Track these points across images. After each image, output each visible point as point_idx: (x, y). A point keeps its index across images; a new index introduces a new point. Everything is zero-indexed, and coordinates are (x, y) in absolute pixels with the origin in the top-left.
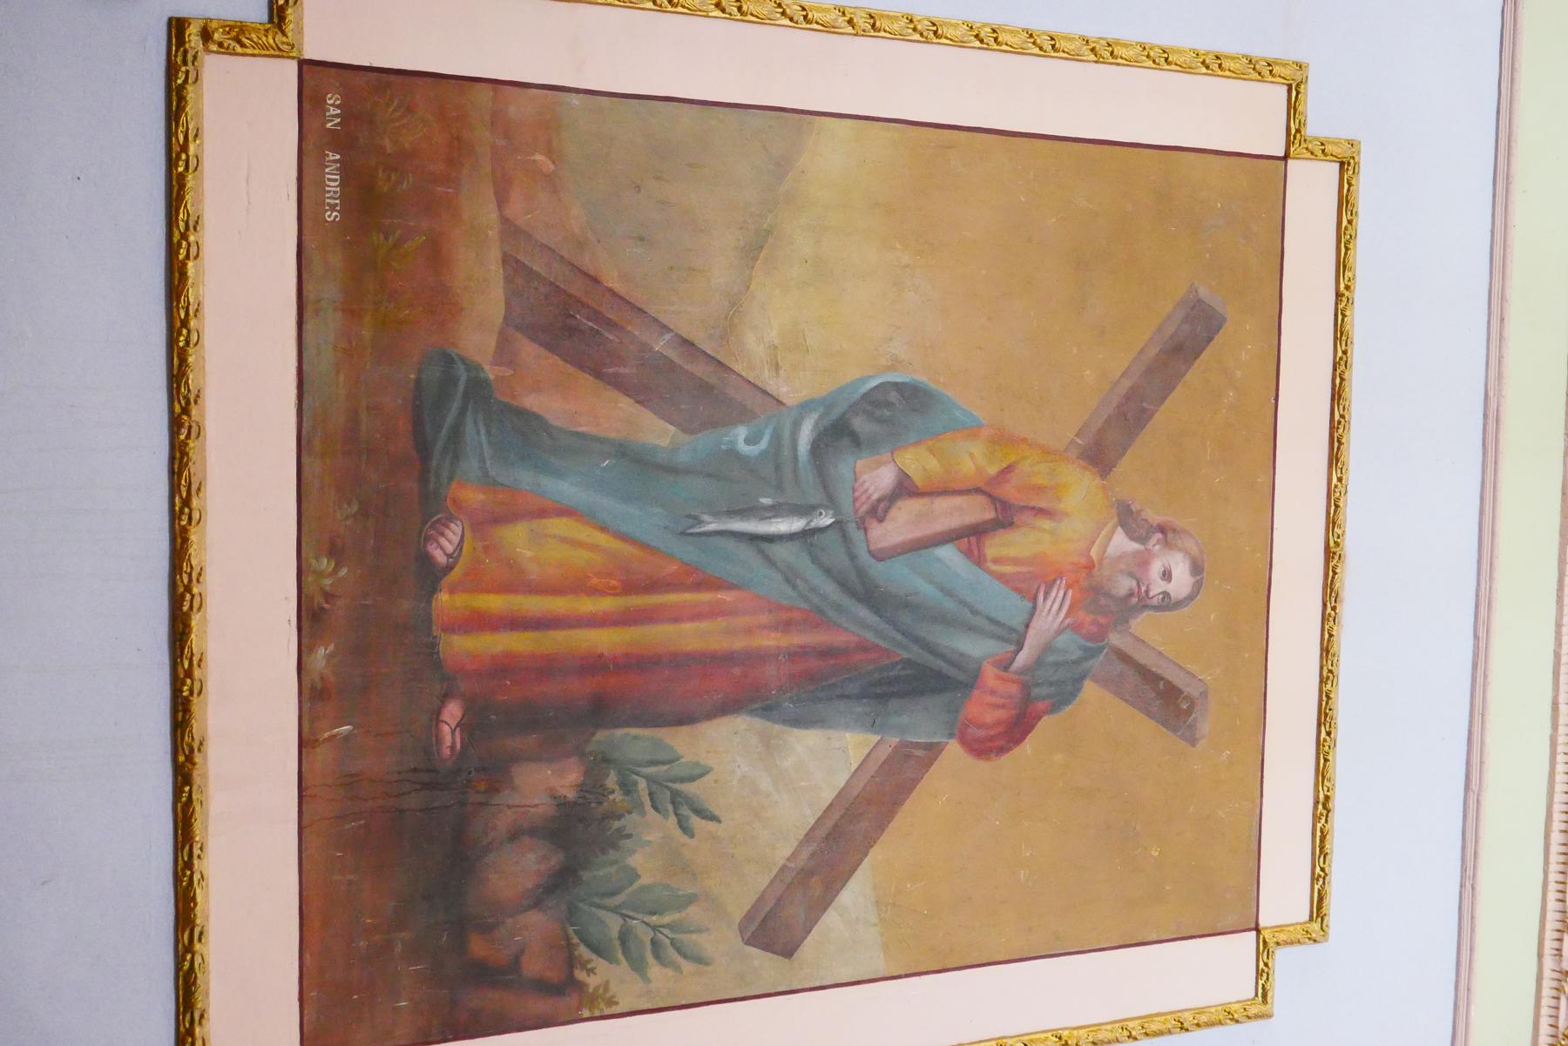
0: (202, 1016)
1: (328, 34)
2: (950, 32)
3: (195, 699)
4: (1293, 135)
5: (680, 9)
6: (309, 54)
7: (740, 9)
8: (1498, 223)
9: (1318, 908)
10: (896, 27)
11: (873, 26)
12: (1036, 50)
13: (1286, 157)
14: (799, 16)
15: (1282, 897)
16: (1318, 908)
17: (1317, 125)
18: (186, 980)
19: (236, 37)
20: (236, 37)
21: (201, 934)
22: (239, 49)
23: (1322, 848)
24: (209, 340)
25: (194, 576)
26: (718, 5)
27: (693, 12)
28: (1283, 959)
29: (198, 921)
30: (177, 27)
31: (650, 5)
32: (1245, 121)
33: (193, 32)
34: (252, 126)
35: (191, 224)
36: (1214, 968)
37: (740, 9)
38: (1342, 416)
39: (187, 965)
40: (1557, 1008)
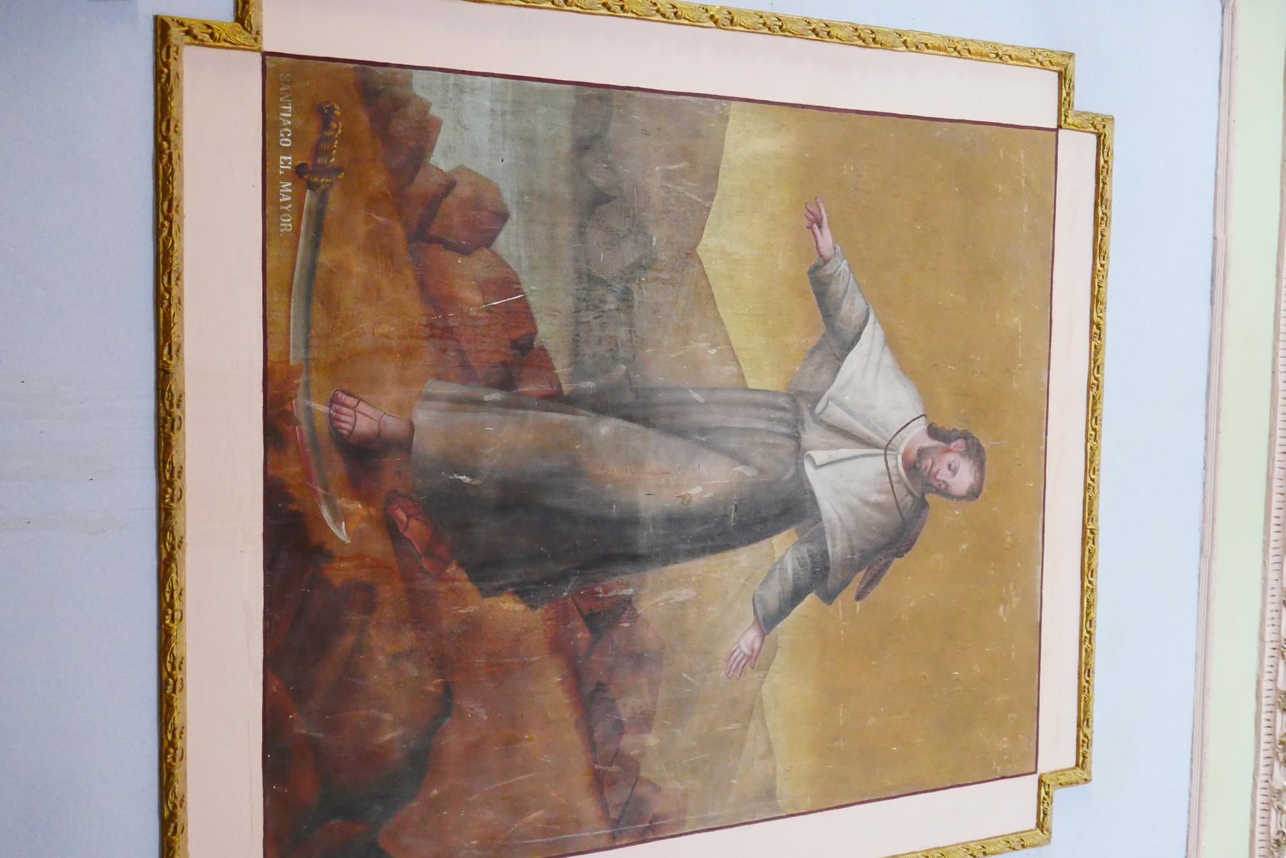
0: (178, 279)
1: (289, 29)
2: (794, 28)
3: (177, 764)
4: (1064, 103)
5: (575, 8)
6: (267, 47)
7: (622, 7)
8: (1219, 192)
9: (1082, 761)
10: (749, 22)
11: (732, 21)
12: (860, 43)
13: (1056, 130)
14: (670, 13)
15: (1056, 750)
16: (1082, 761)
17: (1084, 100)
18: (163, 91)
19: (208, 36)
20: (208, 36)
21: (178, 279)
22: (211, 42)
23: (1094, 411)
24: (191, 830)
25: (175, 401)
26: (604, 5)
27: (584, 10)
28: (1059, 795)
29: (174, 268)
30: (162, 27)
31: (550, 5)
32: (1024, 100)
33: (175, 32)
34: (225, 115)
35: (177, 665)
36: (999, 807)
37: (622, 7)
38: (1106, 162)
39: (165, 233)
40: (1269, 818)
